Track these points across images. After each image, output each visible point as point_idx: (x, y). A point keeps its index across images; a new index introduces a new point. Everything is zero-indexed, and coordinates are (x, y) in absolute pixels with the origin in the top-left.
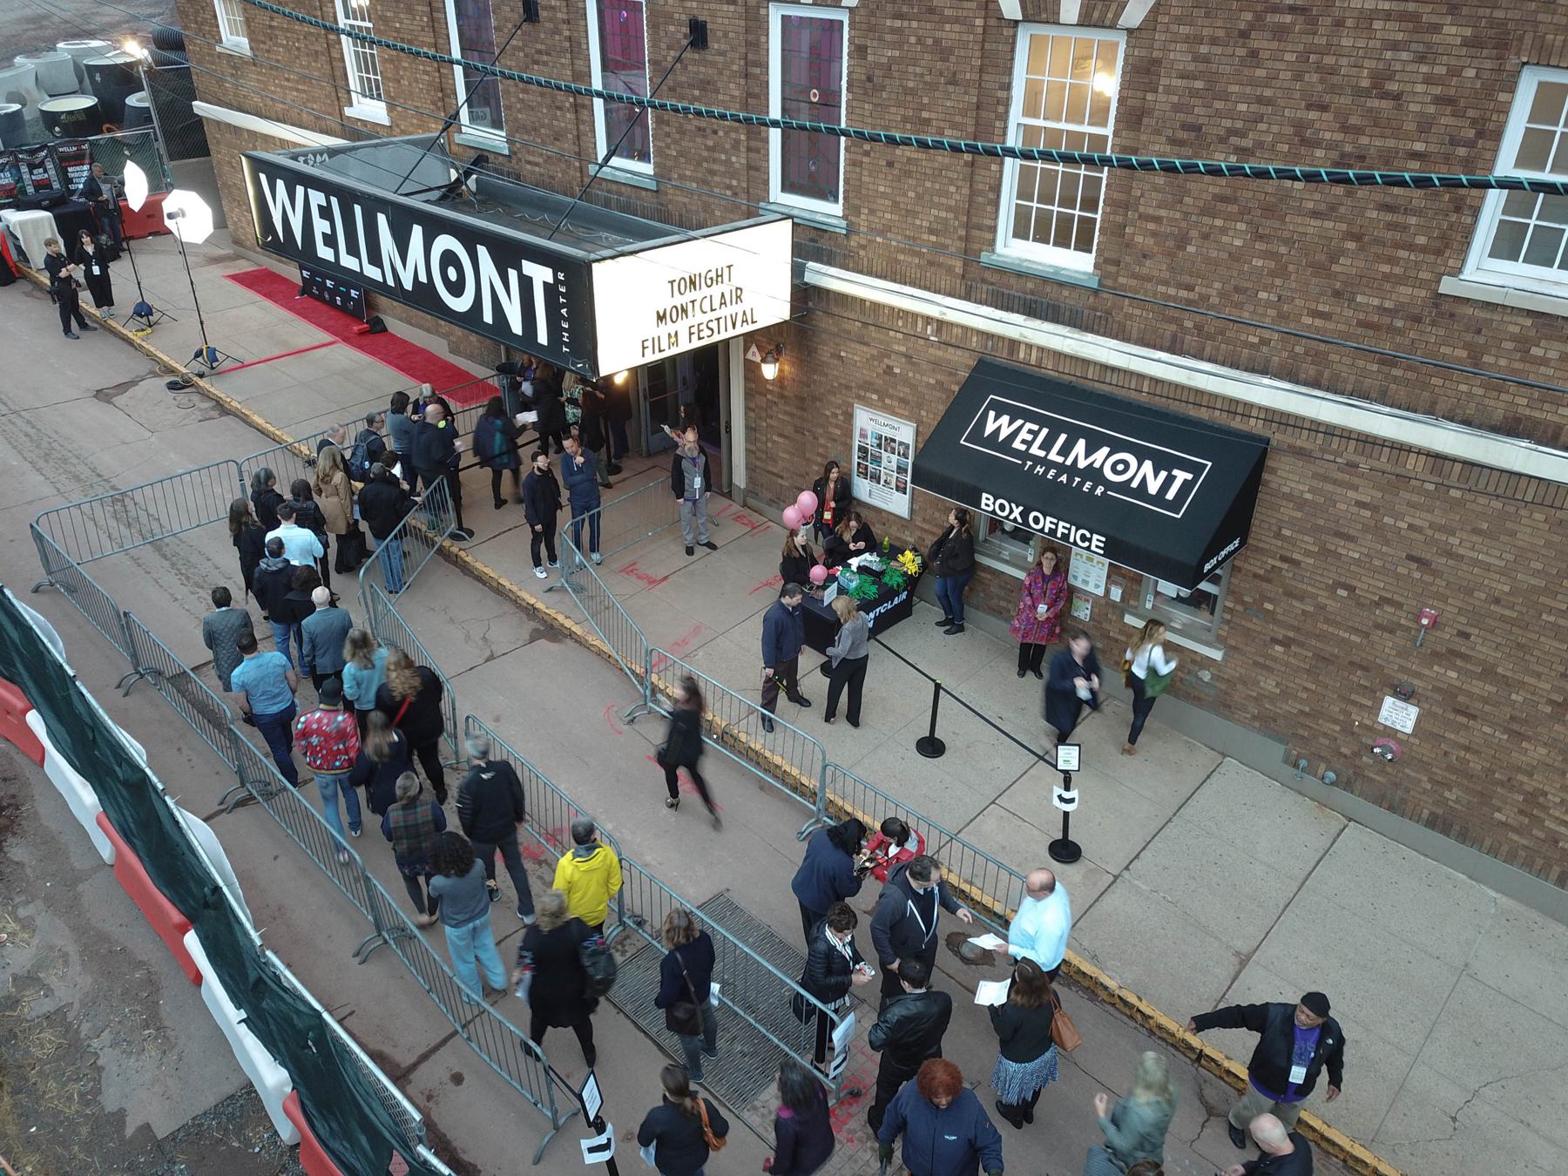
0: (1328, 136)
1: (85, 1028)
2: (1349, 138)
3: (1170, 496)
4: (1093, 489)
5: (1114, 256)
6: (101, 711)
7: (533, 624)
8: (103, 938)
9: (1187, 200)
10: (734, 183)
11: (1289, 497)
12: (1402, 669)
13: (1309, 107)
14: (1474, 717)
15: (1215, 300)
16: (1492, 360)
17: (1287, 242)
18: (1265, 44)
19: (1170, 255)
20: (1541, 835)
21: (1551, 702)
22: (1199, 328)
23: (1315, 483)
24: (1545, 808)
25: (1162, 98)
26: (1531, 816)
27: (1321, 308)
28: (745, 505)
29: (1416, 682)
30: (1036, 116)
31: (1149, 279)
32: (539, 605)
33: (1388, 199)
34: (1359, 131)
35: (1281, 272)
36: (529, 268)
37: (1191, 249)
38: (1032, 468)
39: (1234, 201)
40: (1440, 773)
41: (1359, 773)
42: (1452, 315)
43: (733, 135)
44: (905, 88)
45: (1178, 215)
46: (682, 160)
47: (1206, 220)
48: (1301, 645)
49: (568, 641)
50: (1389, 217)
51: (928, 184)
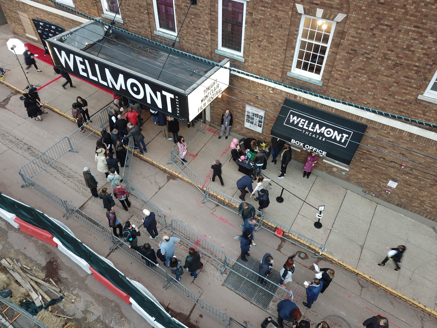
0: (393, 58)
1: (107, 321)
2: (399, 59)
3: (343, 141)
4: (322, 139)
5: (327, 78)
6: (95, 253)
7: (167, 175)
8: (99, 296)
9: (350, 68)
10: (206, 43)
11: (371, 138)
12: (395, 175)
13: (388, 50)
14: (411, 186)
15: (356, 92)
16: (428, 114)
17: (378, 82)
18: (378, 33)
19: (344, 80)
20: (423, 208)
21: (430, 184)
22: (350, 98)
23: (378, 136)
24: (425, 204)
25: (346, 41)
26: (421, 205)
27: (385, 98)
28: (210, 125)
29: (398, 178)
30: (306, 38)
31: (338, 85)
32: (167, 169)
33: (407, 75)
34: (402, 58)
35: (375, 88)
36: (164, 93)
37: (350, 80)
38: (305, 132)
39: (364, 70)
40: (401, 196)
41: (381, 195)
42: (420, 103)
43: (206, 30)
44: (265, 27)
45: (347, 71)
46: (188, 35)
47: (355, 73)
48: (370, 169)
49: (178, 179)
50: (407, 79)
51: (271, 53)
